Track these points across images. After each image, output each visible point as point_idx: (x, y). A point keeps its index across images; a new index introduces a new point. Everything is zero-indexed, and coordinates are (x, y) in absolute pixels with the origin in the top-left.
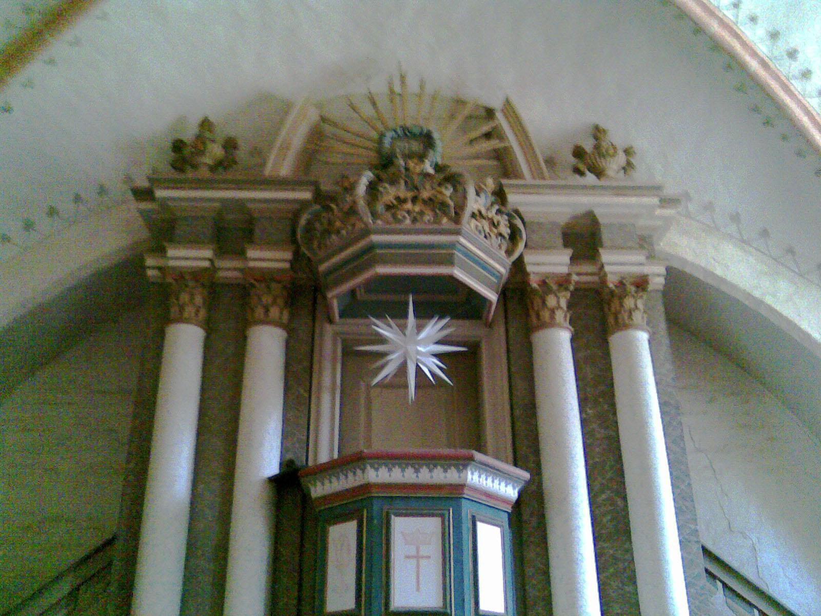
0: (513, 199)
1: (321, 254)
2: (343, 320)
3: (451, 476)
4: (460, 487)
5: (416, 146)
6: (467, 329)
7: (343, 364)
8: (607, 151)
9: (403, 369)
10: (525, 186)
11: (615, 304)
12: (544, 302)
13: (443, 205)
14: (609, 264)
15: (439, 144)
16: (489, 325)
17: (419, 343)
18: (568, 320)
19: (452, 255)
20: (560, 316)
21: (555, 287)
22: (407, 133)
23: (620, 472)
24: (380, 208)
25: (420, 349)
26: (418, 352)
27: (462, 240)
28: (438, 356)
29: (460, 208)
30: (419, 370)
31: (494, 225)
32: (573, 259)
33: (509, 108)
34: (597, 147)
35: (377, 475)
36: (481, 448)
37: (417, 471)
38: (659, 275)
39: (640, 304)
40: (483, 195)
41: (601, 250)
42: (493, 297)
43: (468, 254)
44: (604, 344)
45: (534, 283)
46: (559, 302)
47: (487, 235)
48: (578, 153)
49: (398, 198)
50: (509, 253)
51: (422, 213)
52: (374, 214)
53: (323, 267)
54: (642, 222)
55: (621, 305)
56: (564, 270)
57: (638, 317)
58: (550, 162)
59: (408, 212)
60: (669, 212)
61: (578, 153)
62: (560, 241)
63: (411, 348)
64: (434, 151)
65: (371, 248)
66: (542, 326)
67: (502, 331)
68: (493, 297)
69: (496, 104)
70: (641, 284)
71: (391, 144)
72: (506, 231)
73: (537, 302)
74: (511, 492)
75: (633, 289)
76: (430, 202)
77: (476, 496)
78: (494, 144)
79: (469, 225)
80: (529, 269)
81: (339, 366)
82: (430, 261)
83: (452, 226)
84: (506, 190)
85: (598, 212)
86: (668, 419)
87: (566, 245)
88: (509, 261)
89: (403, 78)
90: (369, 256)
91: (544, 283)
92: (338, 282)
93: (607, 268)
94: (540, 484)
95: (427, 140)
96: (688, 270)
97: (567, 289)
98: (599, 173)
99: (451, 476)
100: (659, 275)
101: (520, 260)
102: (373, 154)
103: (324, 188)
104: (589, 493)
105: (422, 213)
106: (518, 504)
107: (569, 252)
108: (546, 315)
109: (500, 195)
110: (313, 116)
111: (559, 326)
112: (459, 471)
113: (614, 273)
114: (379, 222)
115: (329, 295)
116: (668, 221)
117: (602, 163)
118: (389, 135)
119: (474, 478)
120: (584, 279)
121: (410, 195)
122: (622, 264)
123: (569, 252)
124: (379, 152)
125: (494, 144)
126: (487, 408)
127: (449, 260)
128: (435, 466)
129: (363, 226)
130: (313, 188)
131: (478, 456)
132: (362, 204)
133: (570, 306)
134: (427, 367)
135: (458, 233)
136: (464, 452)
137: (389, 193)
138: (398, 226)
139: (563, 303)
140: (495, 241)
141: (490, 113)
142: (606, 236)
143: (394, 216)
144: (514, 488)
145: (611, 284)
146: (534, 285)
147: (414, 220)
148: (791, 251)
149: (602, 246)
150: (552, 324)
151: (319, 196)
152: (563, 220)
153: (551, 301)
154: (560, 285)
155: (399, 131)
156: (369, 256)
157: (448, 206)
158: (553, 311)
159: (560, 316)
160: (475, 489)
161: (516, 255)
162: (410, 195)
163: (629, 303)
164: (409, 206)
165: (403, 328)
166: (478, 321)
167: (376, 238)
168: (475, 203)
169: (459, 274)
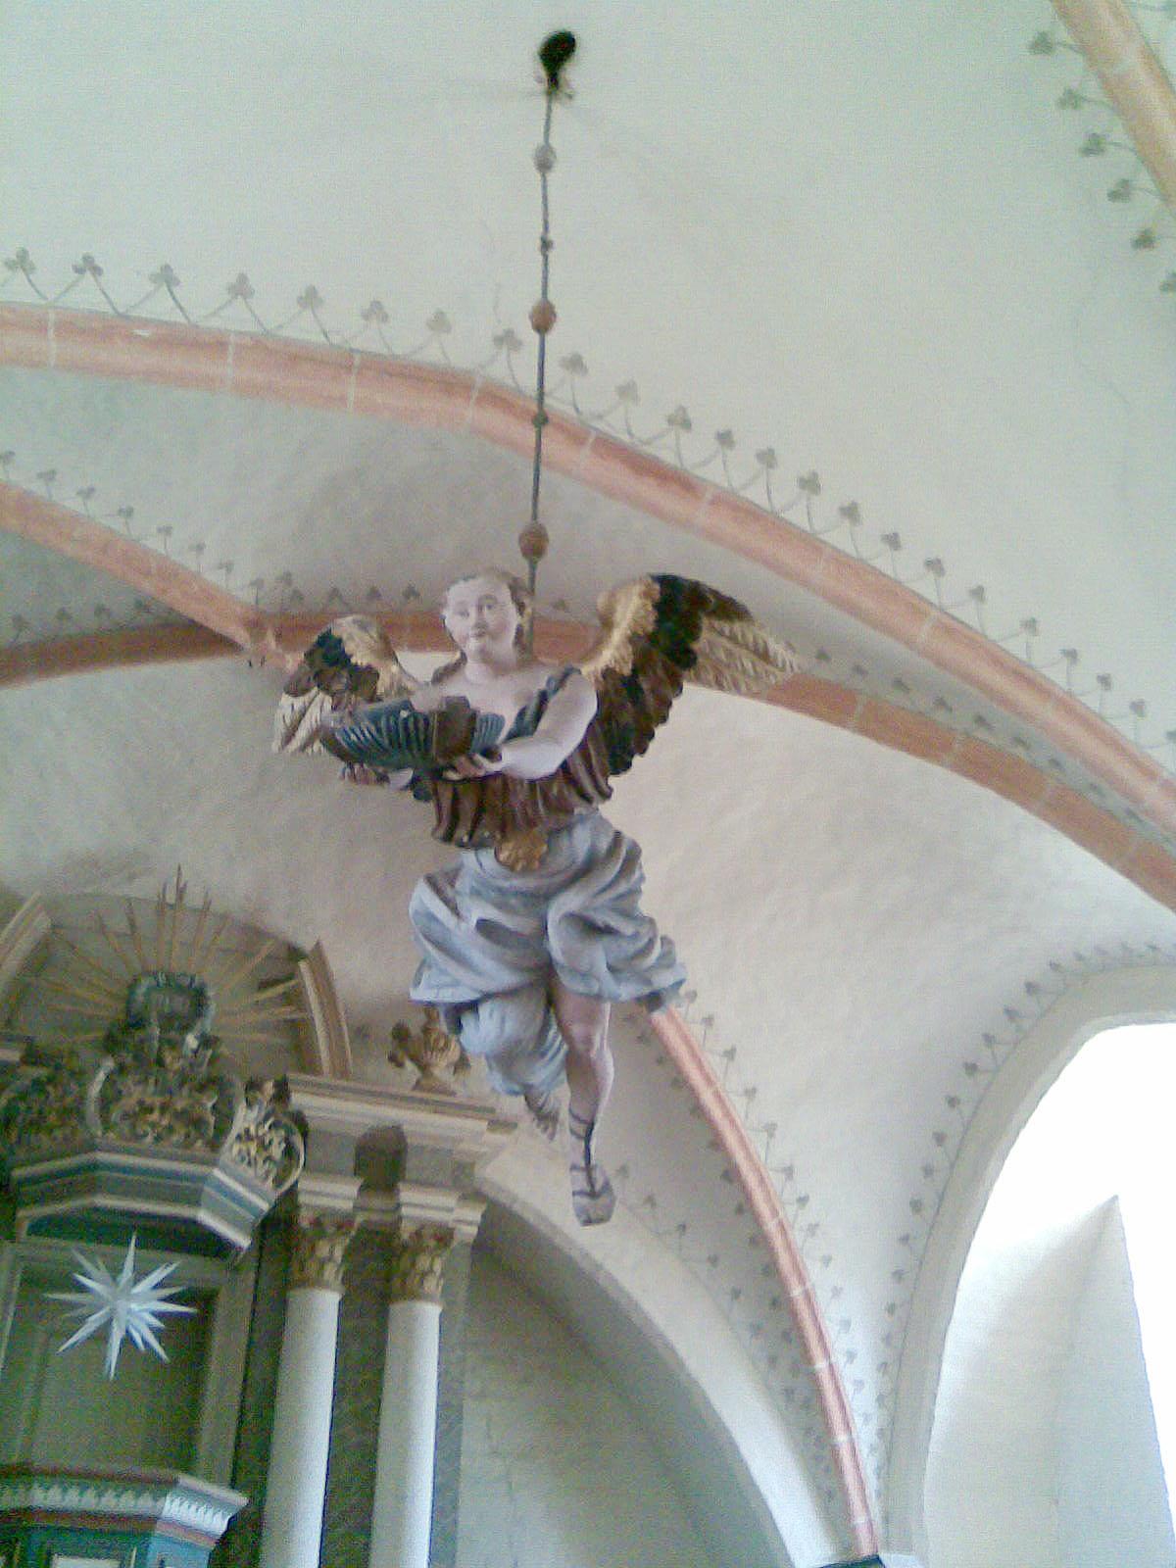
0: (299, 1099)
1: (21, 1154)
2: (34, 1239)
3: (143, 1504)
4: (153, 1520)
5: (181, 1004)
6: (199, 1270)
7: (19, 1307)
8: (437, 1041)
9: (102, 1335)
10: (318, 1085)
11: (405, 1263)
12: (313, 1249)
13: (198, 1123)
14: (409, 1204)
15: (213, 1009)
16: (236, 1270)
17: (130, 1298)
18: (340, 1278)
19: (202, 1190)
20: (330, 1272)
21: (331, 1230)
22: (172, 983)
23: (373, 1476)
24: (115, 1115)
25: (134, 1306)
26: (129, 1312)
27: (217, 1173)
28: (160, 1315)
29: (221, 1131)
30: (128, 1340)
31: (264, 1146)
32: (363, 1189)
33: (318, 958)
34: (426, 1030)
35: (46, 1497)
36: (188, 1470)
37: (100, 1495)
38: (470, 1223)
39: (438, 1266)
40: (256, 1108)
41: (401, 1185)
42: (243, 1241)
43: (221, 1187)
44: (383, 1315)
45: (305, 1219)
46: (333, 1251)
47: (253, 1161)
48: (401, 1034)
49: (141, 1103)
50: (278, 1182)
51: (170, 1129)
52: (107, 1125)
53: (18, 1173)
54: (464, 1146)
55: (413, 1264)
56: (347, 1206)
57: (431, 1285)
58: (361, 1033)
59: (153, 1125)
60: (499, 1138)
61: (401, 1034)
62: (350, 1164)
63: (122, 1305)
64: (158, 1519)
65: (94, 1166)
66: (305, 1283)
67: (252, 1276)
68: (243, 1241)
69: (306, 943)
70: (444, 1237)
71: (147, 994)
72: (277, 1151)
73: (305, 1244)
74: (216, 1523)
75: (432, 1243)
76: (185, 1117)
77: (171, 1532)
78: (286, 1012)
79: (231, 1149)
80: (302, 1199)
81: (12, 1309)
82: (175, 1197)
83: (207, 1154)
84: (291, 1086)
85: (405, 1128)
86: (445, 1426)
87: (357, 1171)
88: (274, 1196)
89: (181, 892)
90: (86, 1178)
91: (317, 1223)
92: (40, 1200)
93: (404, 1211)
94: (261, 1509)
95: (198, 998)
96: (516, 1208)
97: (346, 1234)
98: (424, 1068)
99: (143, 1504)
100: (470, 1223)
101: (292, 1192)
102: (122, 1006)
103: (44, 1038)
104: (324, 1523)
105: (170, 1129)
106: (224, 1541)
107: (359, 1181)
108: (312, 1268)
109: (282, 1093)
110: (42, 923)
111: (327, 1286)
112: (155, 1500)
113: (412, 1219)
114: (111, 1135)
115: (21, 1214)
116: (498, 1149)
117: (429, 1057)
118: (145, 983)
119: (174, 1508)
120: (375, 1217)
121: (157, 1100)
122: (422, 1207)
123: (359, 1181)
124: (129, 1001)
125: (286, 1012)
126: (209, 1403)
127: (194, 1199)
128: (125, 1489)
129: (88, 1136)
130: (24, 1046)
131: (185, 1480)
132: (92, 1109)
133: (348, 1253)
134: (139, 1332)
135: (214, 1163)
136: (165, 1472)
137: (135, 1092)
138: (137, 1145)
139: (338, 1253)
140: (261, 1168)
141: (294, 954)
142: (412, 1163)
143: (133, 1126)
144: (219, 1515)
145: (406, 1231)
146: (305, 1224)
147: (158, 1138)
148: (650, 1200)
149: (404, 1180)
150: (319, 1283)
151: (33, 1057)
152: (358, 1132)
153: (323, 1249)
154: (340, 1227)
155: (162, 979)
156: (86, 1178)
157: (206, 1123)
158: (322, 1263)
159: (330, 1272)
160: (172, 1523)
161: (287, 1186)
162: (157, 1100)
163: (423, 1262)
164: (155, 1116)
165: (115, 1271)
166: (217, 1261)
167: (102, 1157)
168: (245, 1118)
169: (205, 1217)
